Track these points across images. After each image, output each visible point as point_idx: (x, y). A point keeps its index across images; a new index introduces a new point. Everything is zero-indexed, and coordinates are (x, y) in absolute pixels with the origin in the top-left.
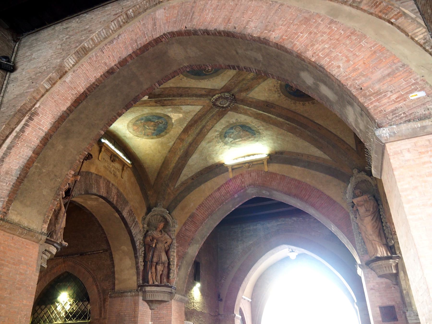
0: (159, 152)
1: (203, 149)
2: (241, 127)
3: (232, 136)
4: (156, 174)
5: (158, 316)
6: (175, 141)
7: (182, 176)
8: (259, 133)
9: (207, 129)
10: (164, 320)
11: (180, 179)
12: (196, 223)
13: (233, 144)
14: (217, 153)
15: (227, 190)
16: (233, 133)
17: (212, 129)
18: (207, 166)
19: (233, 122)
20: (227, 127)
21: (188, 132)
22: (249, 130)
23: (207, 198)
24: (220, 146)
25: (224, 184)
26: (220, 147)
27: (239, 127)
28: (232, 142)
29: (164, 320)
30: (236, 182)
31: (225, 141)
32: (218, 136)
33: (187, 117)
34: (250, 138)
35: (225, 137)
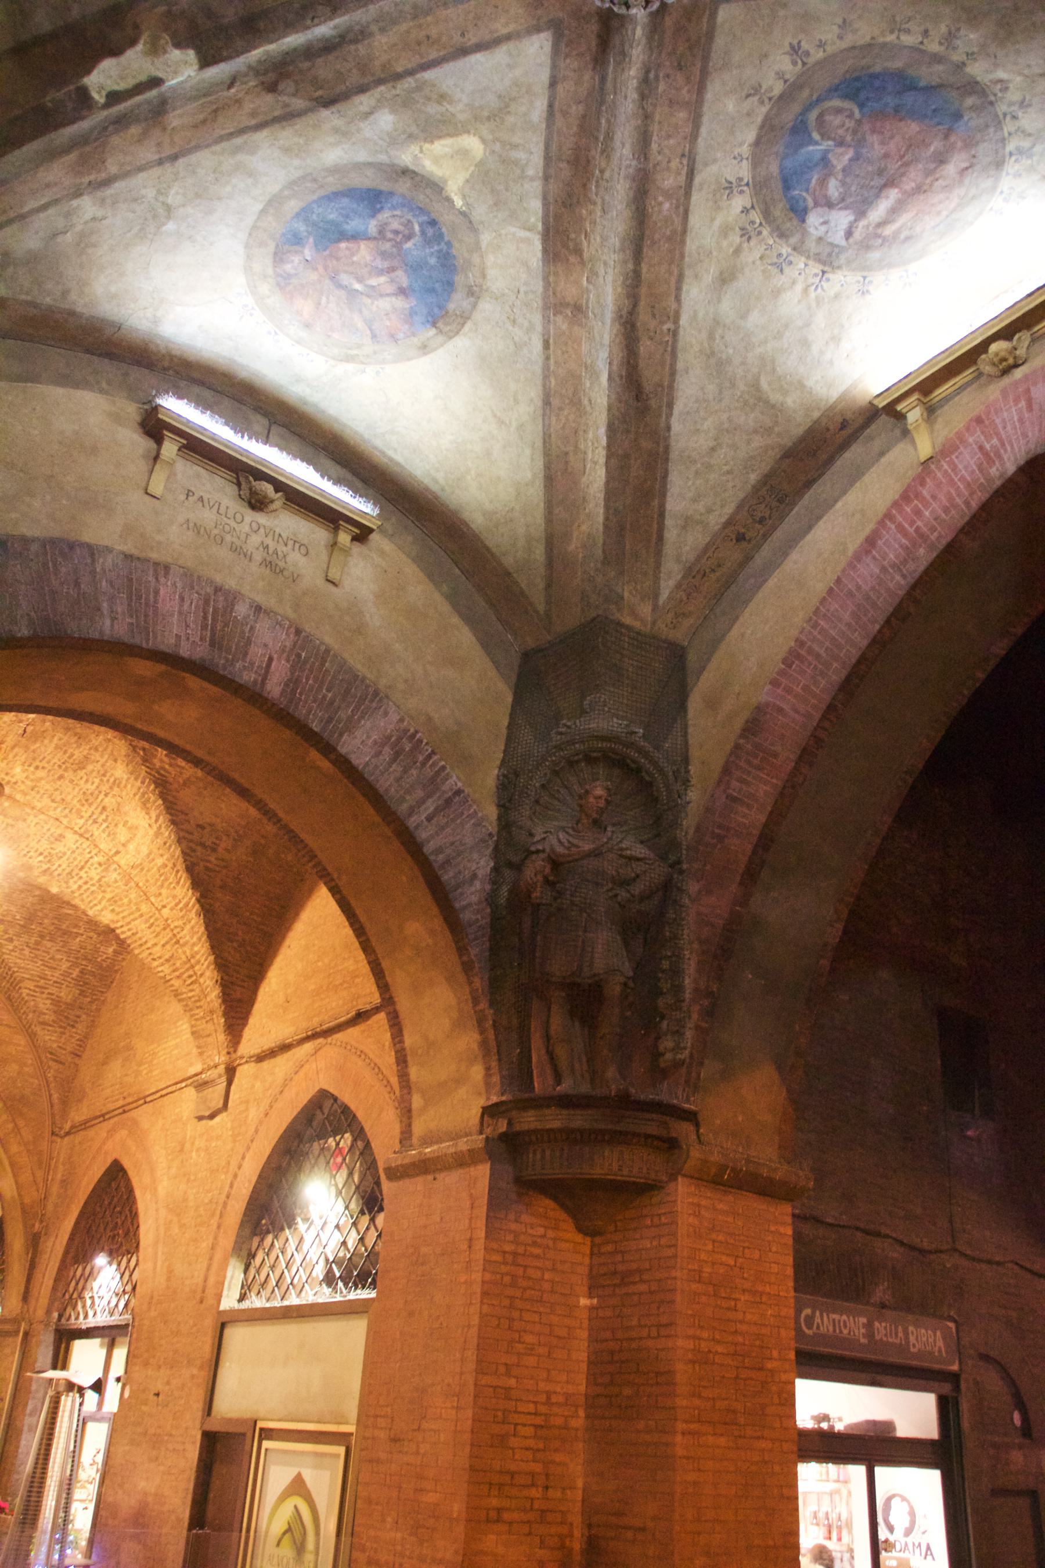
0: (501, 422)
1: (711, 337)
2: (846, 97)
3: (833, 188)
4: (539, 553)
5: (620, 1268)
6: (539, 328)
7: (671, 534)
8: (973, 87)
9: (668, 195)
10: (643, 1287)
11: (669, 549)
12: (775, 755)
13: (866, 246)
14: (805, 343)
15: (911, 530)
16: (824, 160)
17: (697, 180)
18: (787, 442)
19: (780, 75)
20: (768, 130)
21: (578, 252)
22: (909, 98)
23: (816, 612)
24: (799, 287)
25: (896, 504)
26: (806, 290)
27: (836, 103)
28: (858, 235)
29: (643, 1287)
30: (955, 468)
31: (811, 245)
32: (756, 216)
33: (515, 147)
34: (941, 160)
35: (800, 212)
